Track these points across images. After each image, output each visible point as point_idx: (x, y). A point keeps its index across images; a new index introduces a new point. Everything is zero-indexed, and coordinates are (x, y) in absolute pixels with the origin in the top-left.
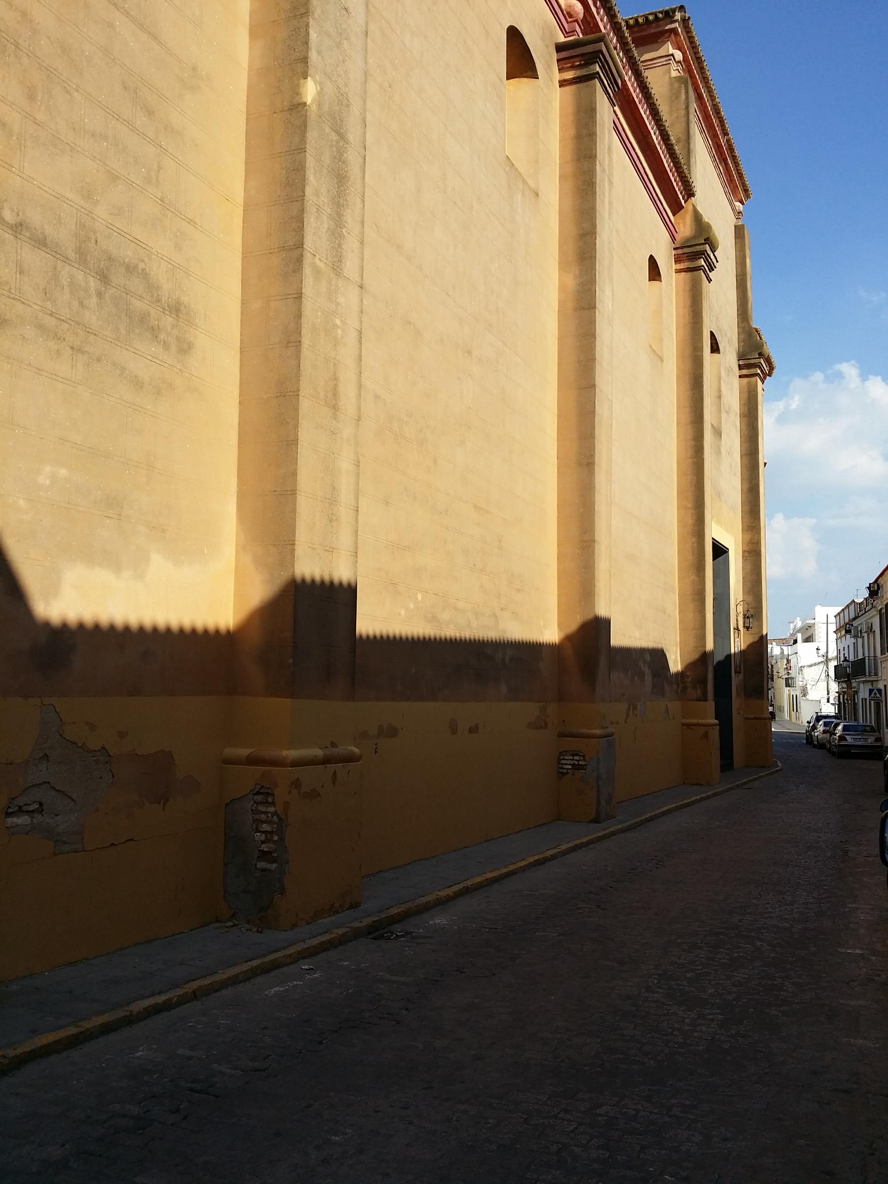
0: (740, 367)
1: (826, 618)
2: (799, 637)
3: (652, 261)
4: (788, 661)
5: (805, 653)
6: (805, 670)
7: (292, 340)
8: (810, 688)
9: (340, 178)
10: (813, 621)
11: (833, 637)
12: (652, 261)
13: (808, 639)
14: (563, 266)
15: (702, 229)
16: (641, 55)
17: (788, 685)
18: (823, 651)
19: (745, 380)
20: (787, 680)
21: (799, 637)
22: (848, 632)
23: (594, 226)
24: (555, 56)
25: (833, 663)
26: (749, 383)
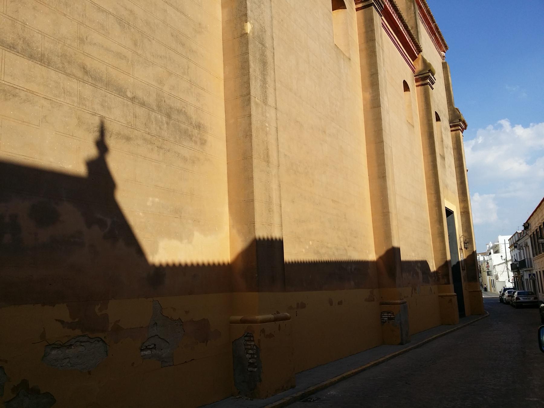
2: (492, 251)
3: (405, 83)
4: (488, 263)
5: (496, 259)
6: (496, 267)
7: (248, 135)
8: (500, 275)
9: (264, 63)
11: (508, 250)
12: (405, 83)
13: (497, 252)
14: (364, 89)
17: (488, 275)
18: (504, 257)
19: (454, 132)
22: (515, 247)
23: (377, 70)
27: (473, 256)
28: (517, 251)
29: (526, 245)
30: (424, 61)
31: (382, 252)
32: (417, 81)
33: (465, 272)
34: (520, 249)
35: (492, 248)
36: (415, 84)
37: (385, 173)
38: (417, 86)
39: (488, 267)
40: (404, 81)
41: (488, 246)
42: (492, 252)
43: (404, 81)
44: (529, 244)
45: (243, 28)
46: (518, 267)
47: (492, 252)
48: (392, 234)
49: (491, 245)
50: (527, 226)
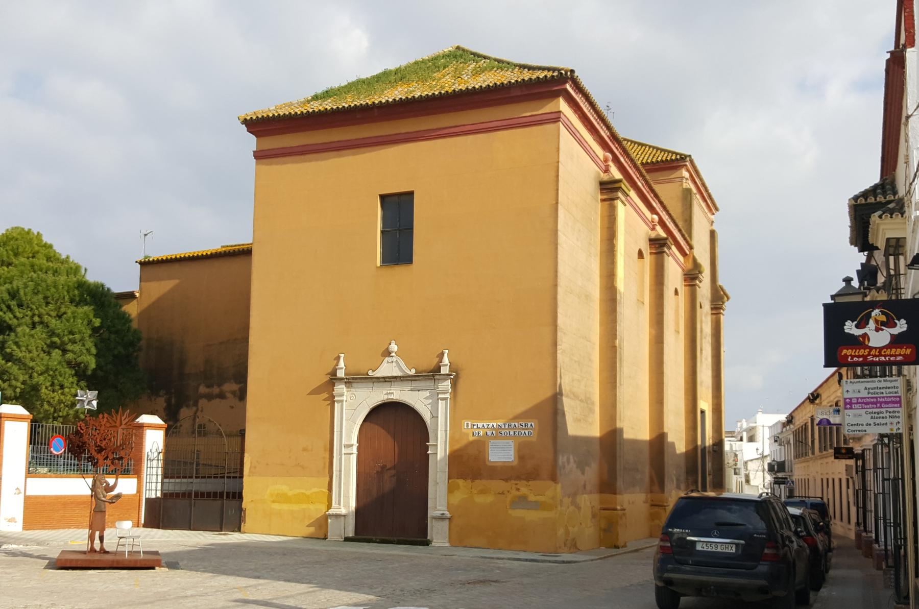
13: (751, 439)
17: (736, 474)
18: (760, 451)
22: (776, 441)
28: (776, 446)
29: (788, 443)
31: (654, 436)
33: (708, 462)
34: (780, 445)
36: (600, 197)
38: (602, 200)
39: (736, 461)
40: (246, 122)
42: (745, 438)
43: (246, 122)
44: (792, 442)
45: (614, 343)
46: (777, 468)
47: (745, 438)
49: (745, 426)
50: (790, 420)
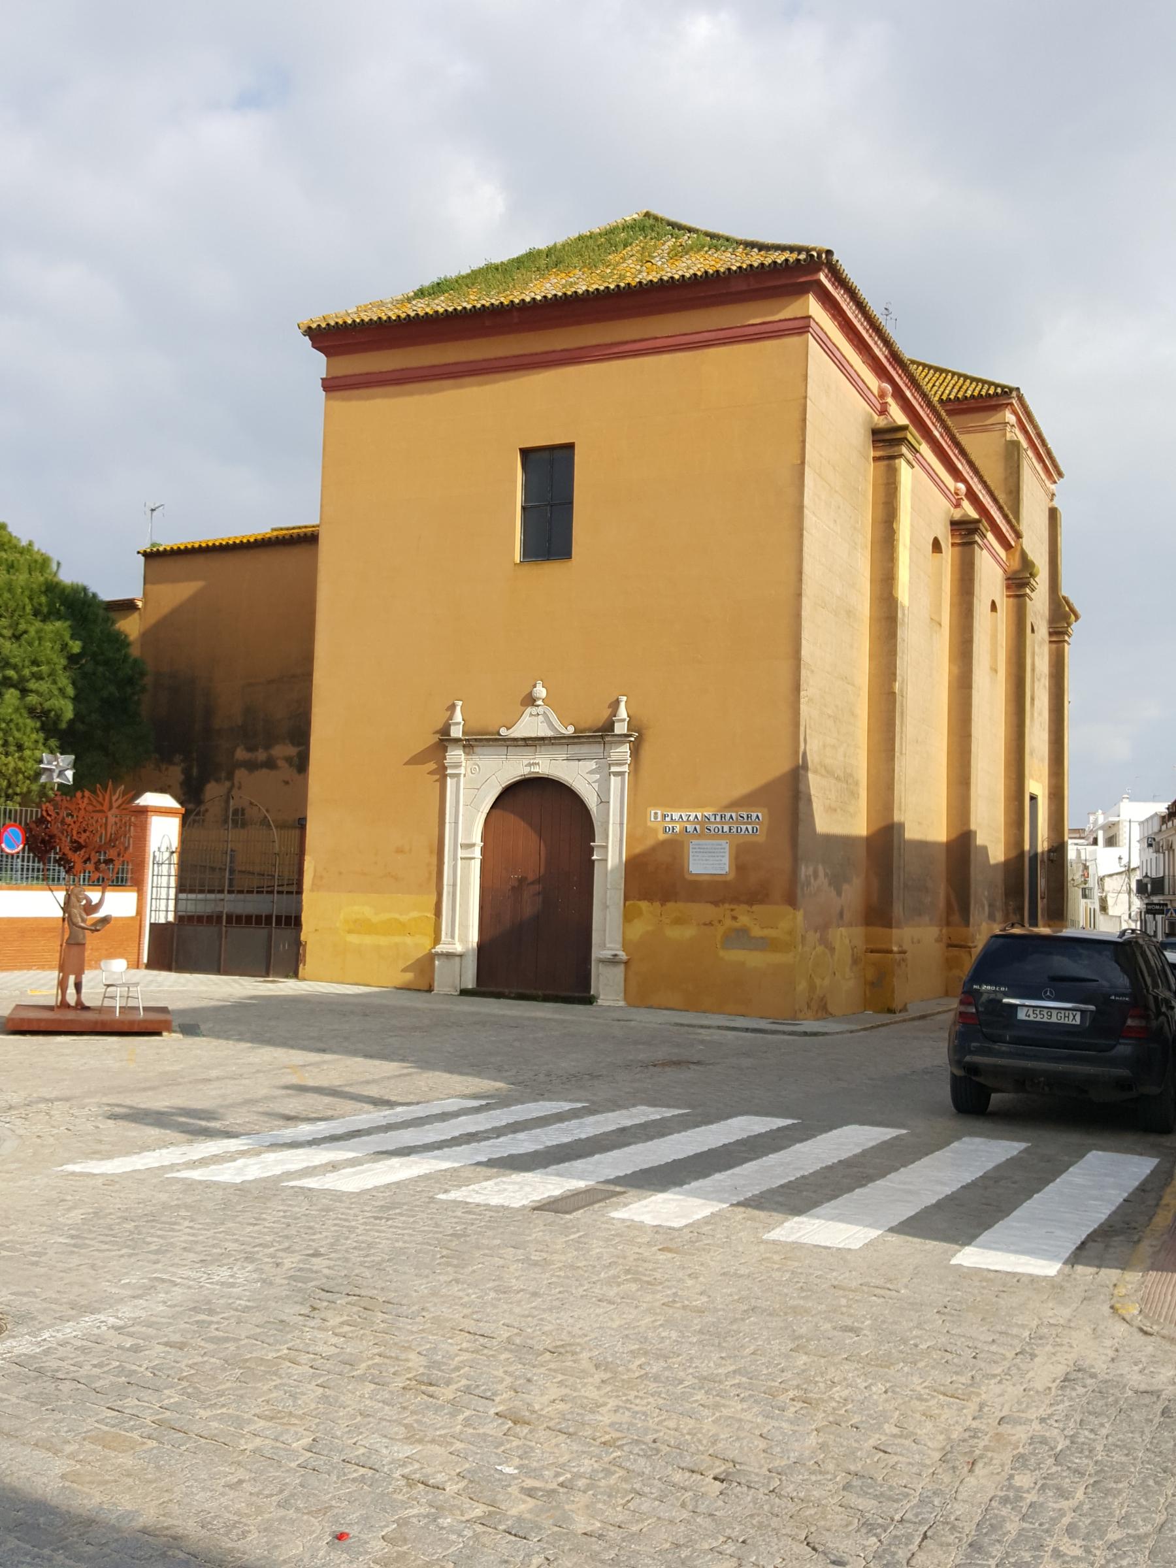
0: (1051, 634)
1: (1138, 814)
2: (1101, 836)
3: (993, 603)
4: (1086, 868)
5: (1105, 861)
6: (1107, 880)
7: (890, 786)
8: (1109, 906)
9: (902, 713)
10: (1116, 819)
11: (1136, 847)
12: (993, 603)
13: (1111, 842)
14: (951, 660)
15: (1027, 564)
16: (1074, 924)
17: (1085, 896)
18: (1125, 861)
19: (1054, 646)
20: (1084, 890)
21: (1101, 836)
22: (1150, 845)
23: (972, 637)
24: (949, 528)
25: (1137, 876)
26: (1058, 649)
27: (1058, 850)
30: (1024, 555)
32: (1008, 587)
33: (1040, 877)
35: (1102, 828)
37: (969, 778)
41: (1092, 818)
42: (1101, 841)
48: (626, 321)
